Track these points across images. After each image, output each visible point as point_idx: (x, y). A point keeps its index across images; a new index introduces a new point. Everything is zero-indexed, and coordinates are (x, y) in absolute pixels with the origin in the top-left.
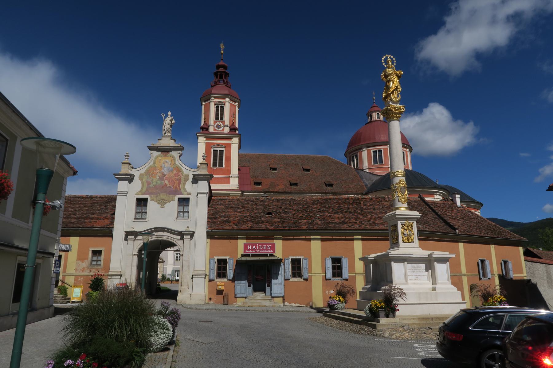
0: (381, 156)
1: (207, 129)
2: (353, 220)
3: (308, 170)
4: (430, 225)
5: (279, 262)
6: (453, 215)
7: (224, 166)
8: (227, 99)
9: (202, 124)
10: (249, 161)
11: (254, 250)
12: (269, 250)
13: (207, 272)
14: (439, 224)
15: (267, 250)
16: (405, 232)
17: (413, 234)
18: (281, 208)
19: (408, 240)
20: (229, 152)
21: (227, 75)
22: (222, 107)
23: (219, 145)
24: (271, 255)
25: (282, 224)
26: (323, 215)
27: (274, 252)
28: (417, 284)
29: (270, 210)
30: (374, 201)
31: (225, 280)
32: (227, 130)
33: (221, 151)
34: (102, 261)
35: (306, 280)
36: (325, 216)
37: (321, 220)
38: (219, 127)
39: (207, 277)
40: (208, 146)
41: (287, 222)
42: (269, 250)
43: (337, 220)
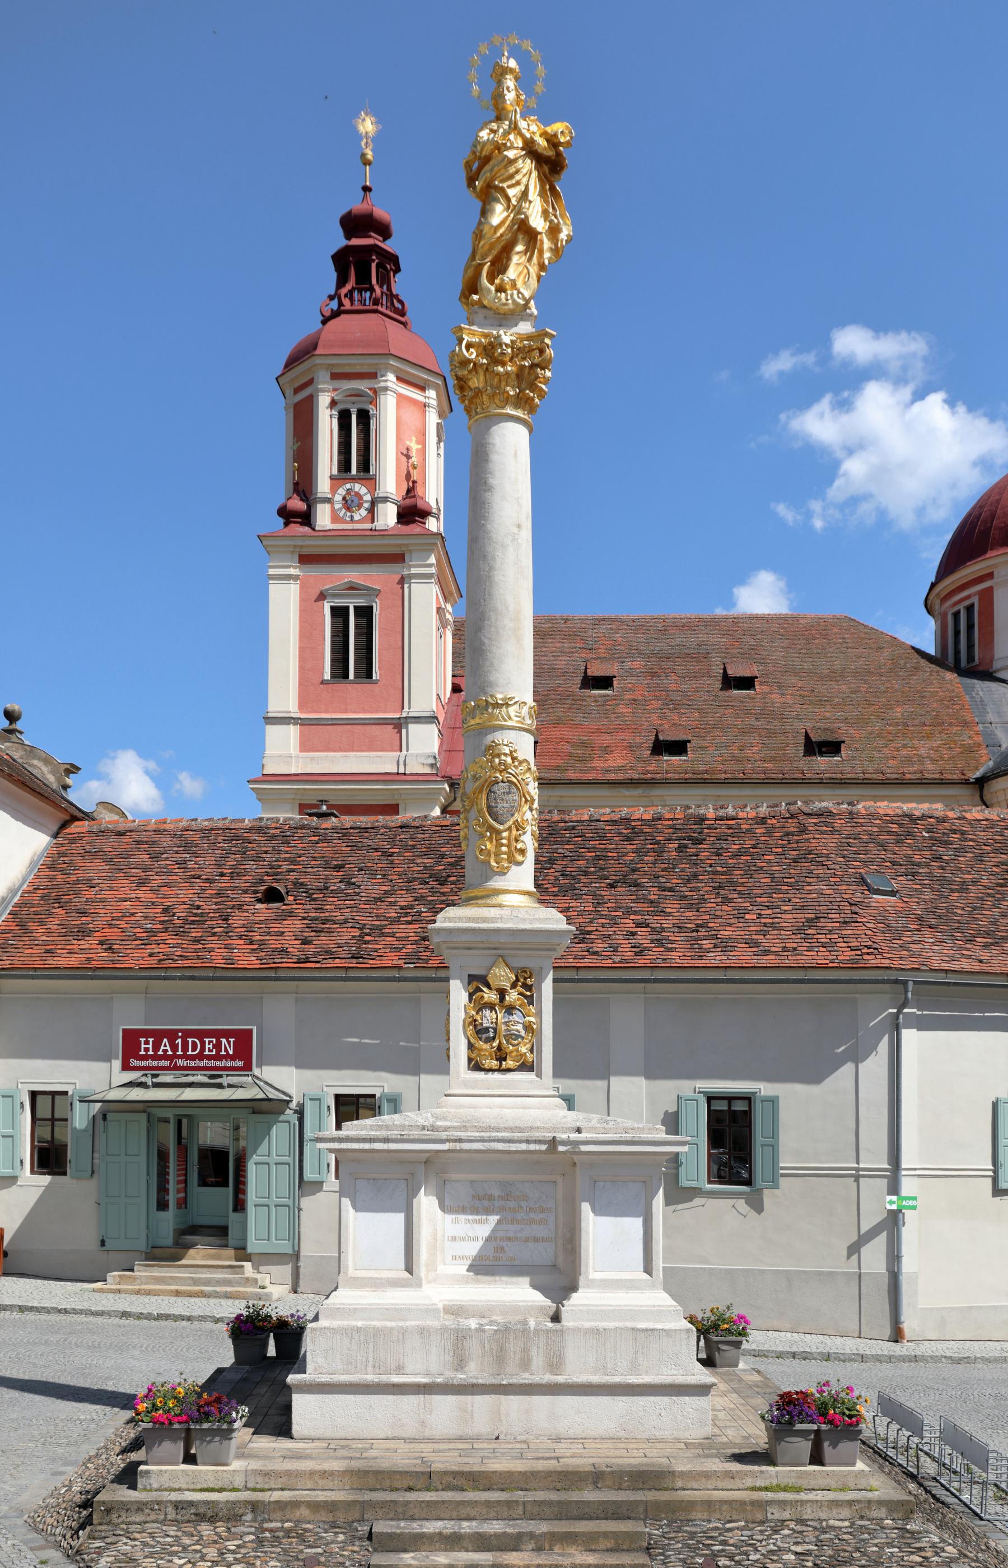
3: (747, 683)
11: (165, 1057)
12: (228, 1057)
15: (218, 1057)
16: (487, 1018)
19: (501, 1059)
22: (364, 417)
32: (388, 516)
42: (228, 1057)
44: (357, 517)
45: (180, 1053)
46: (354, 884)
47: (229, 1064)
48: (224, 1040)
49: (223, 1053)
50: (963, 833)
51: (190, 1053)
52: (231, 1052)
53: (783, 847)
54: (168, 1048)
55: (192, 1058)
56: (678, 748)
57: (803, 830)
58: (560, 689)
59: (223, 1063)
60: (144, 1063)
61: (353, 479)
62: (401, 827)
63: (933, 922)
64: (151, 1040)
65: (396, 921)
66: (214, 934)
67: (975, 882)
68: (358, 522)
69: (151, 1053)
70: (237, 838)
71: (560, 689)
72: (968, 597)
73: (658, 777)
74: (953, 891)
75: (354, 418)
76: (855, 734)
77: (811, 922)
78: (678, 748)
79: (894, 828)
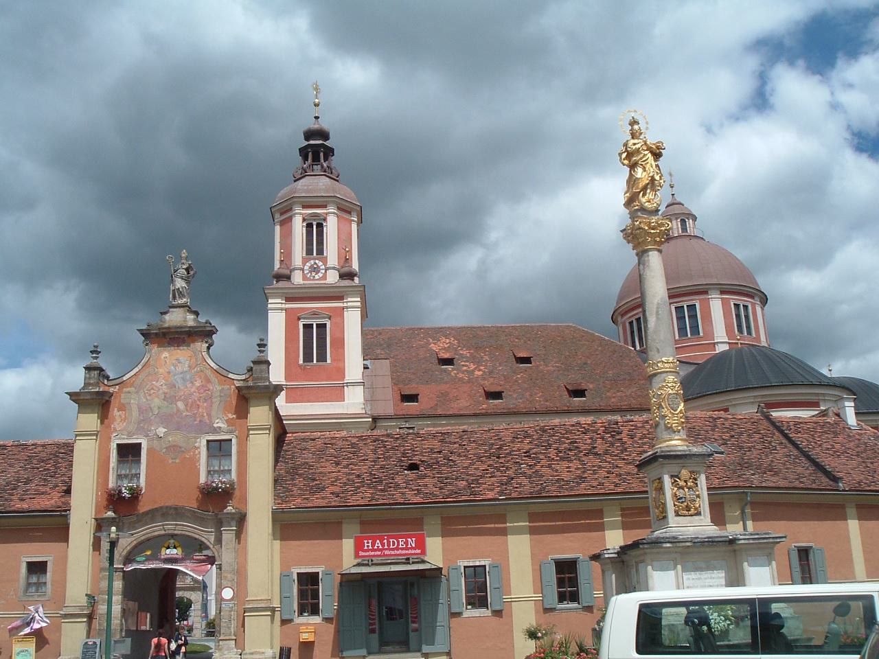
0: (693, 317)
1: (288, 278)
2: (603, 473)
3: (527, 360)
4: (776, 474)
5: (434, 575)
6: (838, 446)
7: (329, 361)
8: (332, 209)
9: (277, 265)
10: (389, 346)
11: (378, 549)
12: (412, 548)
13: (276, 604)
14: (800, 470)
15: (407, 549)
16: (680, 493)
17: (698, 496)
18: (440, 452)
20: (341, 328)
21: (329, 152)
22: (320, 226)
23: (315, 314)
24: (423, 562)
25: (441, 488)
27: (424, 553)
28: (139, 532)
29: (416, 460)
31: (316, 620)
32: (333, 278)
34: (49, 586)
35: (498, 613)
36: (537, 468)
38: (315, 269)
39: (277, 614)
40: (292, 319)
42: (412, 548)
43: (565, 476)
44: (317, 277)
45: (386, 547)
46: (451, 460)
47: (413, 552)
48: (409, 540)
49: (409, 546)
50: (737, 425)
51: (391, 547)
52: (414, 546)
54: (379, 545)
55: (393, 549)
56: (497, 395)
58: (423, 366)
59: (410, 552)
60: (367, 554)
61: (315, 259)
62: (463, 432)
64: (370, 541)
65: (482, 477)
68: (317, 280)
69: (370, 548)
71: (423, 366)
72: (637, 314)
75: (315, 227)
76: (591, 386)
78: (497, 395)
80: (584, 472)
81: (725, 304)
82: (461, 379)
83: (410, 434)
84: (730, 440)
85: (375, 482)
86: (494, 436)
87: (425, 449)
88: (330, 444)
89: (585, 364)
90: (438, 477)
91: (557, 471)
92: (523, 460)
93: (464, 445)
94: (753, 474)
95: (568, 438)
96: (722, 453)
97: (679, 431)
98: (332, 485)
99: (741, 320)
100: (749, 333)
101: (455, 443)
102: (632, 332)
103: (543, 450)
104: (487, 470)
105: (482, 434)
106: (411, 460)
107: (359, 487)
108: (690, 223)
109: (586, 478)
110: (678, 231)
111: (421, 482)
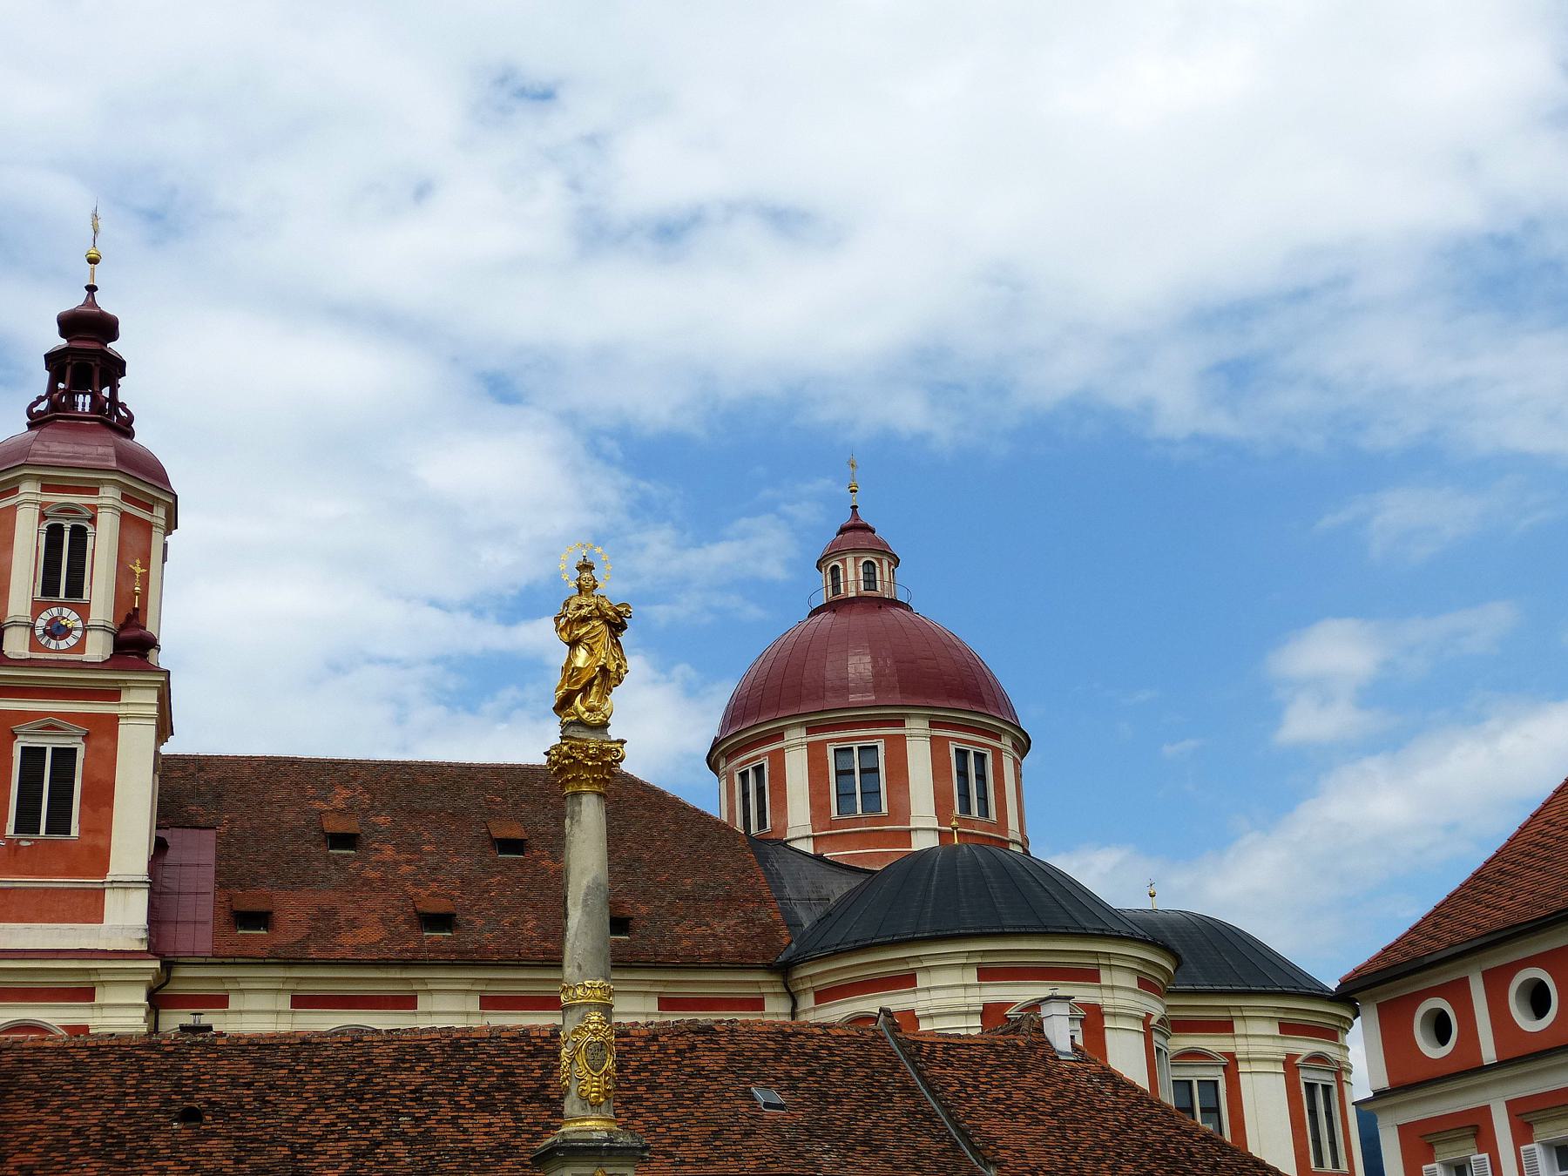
3: (512, 845)
6: (1018, 1096)
7: (75, 831)
18: (248, 1085)
20: (106, 759)
22: (79, 535)
23: (50, 725)
25: (238, 1161)
26: (427, 1117)
30: (663, 1048)
32: (98, 648)
33: (65, 757)
36: (431, 1123)
37: (413, 1141)
38: (57, 630)
41: (258, 1151)
43: (480, 1141)
50: (829, 1048)
53: (677, 1063)
57: (693, 1048)
61: (62, 605)
63: (820, 1133)
65: (322, 1138)
66: (139, 1156)
67: (848, 1095)
70: (130, 1056)
73: (420, 956)
74: (829, 1103)
76: (644, 909)
77: (716, 1135)
78: (441, 921)
79: (771, 1045)
80: (515, 1136)
81: (938, 745)
82: (367, 882)
83: (197, 1044)
84: (804, 1080)
85: (112, 1145)
86: (360, 1055)
87: (220, 1077)
88: (29, 1061)
89: (639, 859)
90: (238, 1138)
91: (465, 1131)
92: (406, 1107)
93: (299, 1072)
94: (826, 1152)
95: (499, 1066)
96: (781, 1107)
97: (600, 1105)
98: (23, 1151)
99: (965, 781)
100: (984, 811)
101: (282, 1067)
102: (745, 796)
103: (449, 1087)
104: (335, 1125)
105: (338, 1049)
106: (188, 1100)
107: (75, 1156)
108: (883, 571)
109: (516, 1147)
110: (857, 587)
111: (202, 1147)
